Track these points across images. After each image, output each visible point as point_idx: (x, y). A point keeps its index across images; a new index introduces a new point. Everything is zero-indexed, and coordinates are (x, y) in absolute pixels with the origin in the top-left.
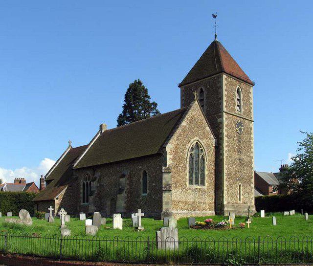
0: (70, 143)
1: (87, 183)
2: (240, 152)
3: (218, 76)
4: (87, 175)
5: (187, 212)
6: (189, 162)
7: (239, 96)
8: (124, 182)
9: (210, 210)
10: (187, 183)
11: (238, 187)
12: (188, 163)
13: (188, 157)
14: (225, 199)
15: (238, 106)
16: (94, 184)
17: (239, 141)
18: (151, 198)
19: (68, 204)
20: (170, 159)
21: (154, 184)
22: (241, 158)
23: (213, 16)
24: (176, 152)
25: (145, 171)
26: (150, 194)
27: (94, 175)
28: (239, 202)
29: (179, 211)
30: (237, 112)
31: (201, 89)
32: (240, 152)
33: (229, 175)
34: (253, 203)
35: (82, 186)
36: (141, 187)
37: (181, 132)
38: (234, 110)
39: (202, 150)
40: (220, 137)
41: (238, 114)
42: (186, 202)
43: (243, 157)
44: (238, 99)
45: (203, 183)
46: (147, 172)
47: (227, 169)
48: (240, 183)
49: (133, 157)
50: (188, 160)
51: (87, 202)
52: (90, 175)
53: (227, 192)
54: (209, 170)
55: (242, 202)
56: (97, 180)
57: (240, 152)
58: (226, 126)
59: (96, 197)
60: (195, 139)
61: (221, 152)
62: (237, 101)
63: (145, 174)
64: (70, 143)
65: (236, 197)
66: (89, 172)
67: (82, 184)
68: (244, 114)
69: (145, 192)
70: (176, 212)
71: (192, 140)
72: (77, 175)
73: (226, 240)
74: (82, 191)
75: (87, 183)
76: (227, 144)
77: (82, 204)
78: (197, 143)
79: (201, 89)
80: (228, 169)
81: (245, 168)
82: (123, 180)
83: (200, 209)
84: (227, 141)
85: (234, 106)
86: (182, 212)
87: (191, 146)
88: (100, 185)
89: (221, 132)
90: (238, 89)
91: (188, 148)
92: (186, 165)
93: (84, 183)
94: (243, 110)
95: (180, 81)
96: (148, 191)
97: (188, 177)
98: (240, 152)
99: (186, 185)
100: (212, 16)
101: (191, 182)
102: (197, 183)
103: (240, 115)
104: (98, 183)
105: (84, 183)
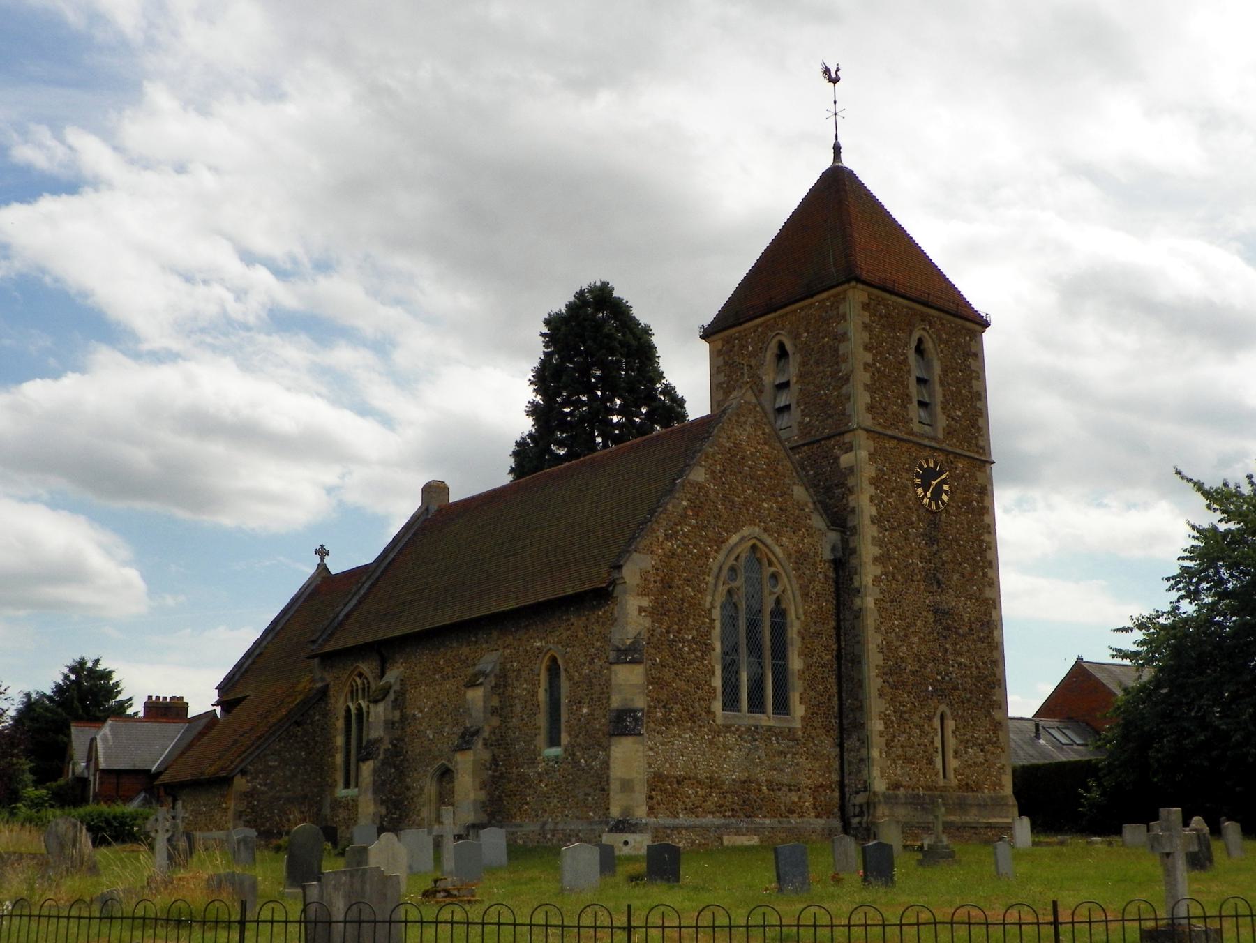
0: (322, 552)
1: (360, 709)
2: (939, 583)
3: (835, 296)
4: (360, 675)
5: (719, 821)
6: (723, 624)
7: (928, 366)
8: (481, 704)
9: (817, 817)
10: (717, 706)
11: (936, 723)
12: (718, 624)
13: (718, 604)
14: (876, 772)
15: (922, 404)
16: (378, 713)
17: (932, 541)
18: (577, 763)
19: (284, 794)
20: (641, 609)
21: (585, 711)
22: (944, 606)
23: (827, 71)
24: (667, 585)
25: (554, 660)
26: (570, 750)
27: (383, 674)
28: (941, 782)
29: (683, 819)
30: (916, 427)
31: (781, 346)
32: (939, 583)
33: (893, 674)
34: (1008, 790)
35: (340, 724)
36: (542, 720)
37: (685, 508)
38: (908, 421)
39: (775, 577)
40: (850, 524)
41: (923, 436)
42: (713, 783)
43: (948, 600)
44: (921, 381)
45: (782, 706)
46: (560, 662)
47: (881, 651)
48: (943, 708)
49: (510, 606)
50: (716, 613)
51: (357, 786)
52: (371, 680)
53: (883, 740)
54: (806, 653)
55: (954, 782)
56: (392, 696)
57: (935, 581)
58: (875, 482)
59: (384, 763)
60: (746, 531)
61: (856, 584)
62: (913, 388)
63: (554, 670)
64: (322, 552)
65: (931, 762)
66: (364, 667)
67: (342, 713)
68: (949, 433)
69: (554, 741)
70: (669, 821)
71: (735, 538)
72: (328, 680)
73: (925, 916)
74: (340, 740)
75: (360, 709)
76: (877, 551)
77: (341, 792)
78: (754, 547)
79: (781, 346)
80: (888, 650)
81: (964, 646)
82: (476, 696)
83: (774, 812)
84: (877, 542)
85: (904, 406)
86: (697, 821)
87: (731, 561)
88: (403, 718)
89: (852, 504)
90: (920, 341)
91: (715, 570)
92: (708, 634)
93: (348, 710)
94: (942, 421)
95: (708, 318)
96: (565, 739)
97: (717, 682)
98: (935, 581)
99: (709, 712)
100: (820, 72)
101: (731, 702)
102: (757, 705)
103: (934, 439)
104: (394, 708)
105: (348, 710)
